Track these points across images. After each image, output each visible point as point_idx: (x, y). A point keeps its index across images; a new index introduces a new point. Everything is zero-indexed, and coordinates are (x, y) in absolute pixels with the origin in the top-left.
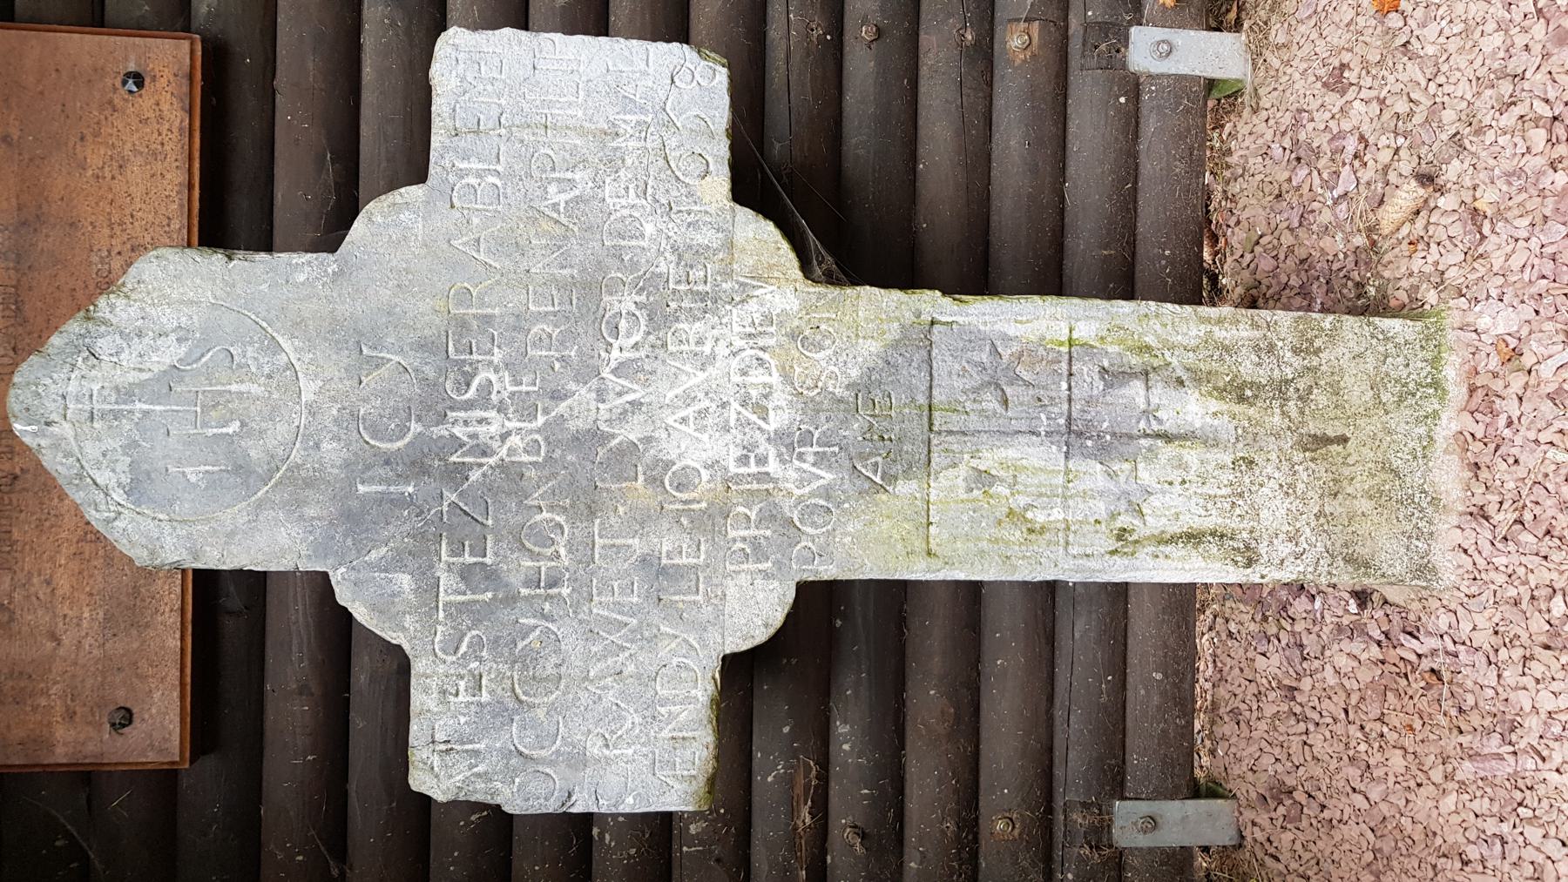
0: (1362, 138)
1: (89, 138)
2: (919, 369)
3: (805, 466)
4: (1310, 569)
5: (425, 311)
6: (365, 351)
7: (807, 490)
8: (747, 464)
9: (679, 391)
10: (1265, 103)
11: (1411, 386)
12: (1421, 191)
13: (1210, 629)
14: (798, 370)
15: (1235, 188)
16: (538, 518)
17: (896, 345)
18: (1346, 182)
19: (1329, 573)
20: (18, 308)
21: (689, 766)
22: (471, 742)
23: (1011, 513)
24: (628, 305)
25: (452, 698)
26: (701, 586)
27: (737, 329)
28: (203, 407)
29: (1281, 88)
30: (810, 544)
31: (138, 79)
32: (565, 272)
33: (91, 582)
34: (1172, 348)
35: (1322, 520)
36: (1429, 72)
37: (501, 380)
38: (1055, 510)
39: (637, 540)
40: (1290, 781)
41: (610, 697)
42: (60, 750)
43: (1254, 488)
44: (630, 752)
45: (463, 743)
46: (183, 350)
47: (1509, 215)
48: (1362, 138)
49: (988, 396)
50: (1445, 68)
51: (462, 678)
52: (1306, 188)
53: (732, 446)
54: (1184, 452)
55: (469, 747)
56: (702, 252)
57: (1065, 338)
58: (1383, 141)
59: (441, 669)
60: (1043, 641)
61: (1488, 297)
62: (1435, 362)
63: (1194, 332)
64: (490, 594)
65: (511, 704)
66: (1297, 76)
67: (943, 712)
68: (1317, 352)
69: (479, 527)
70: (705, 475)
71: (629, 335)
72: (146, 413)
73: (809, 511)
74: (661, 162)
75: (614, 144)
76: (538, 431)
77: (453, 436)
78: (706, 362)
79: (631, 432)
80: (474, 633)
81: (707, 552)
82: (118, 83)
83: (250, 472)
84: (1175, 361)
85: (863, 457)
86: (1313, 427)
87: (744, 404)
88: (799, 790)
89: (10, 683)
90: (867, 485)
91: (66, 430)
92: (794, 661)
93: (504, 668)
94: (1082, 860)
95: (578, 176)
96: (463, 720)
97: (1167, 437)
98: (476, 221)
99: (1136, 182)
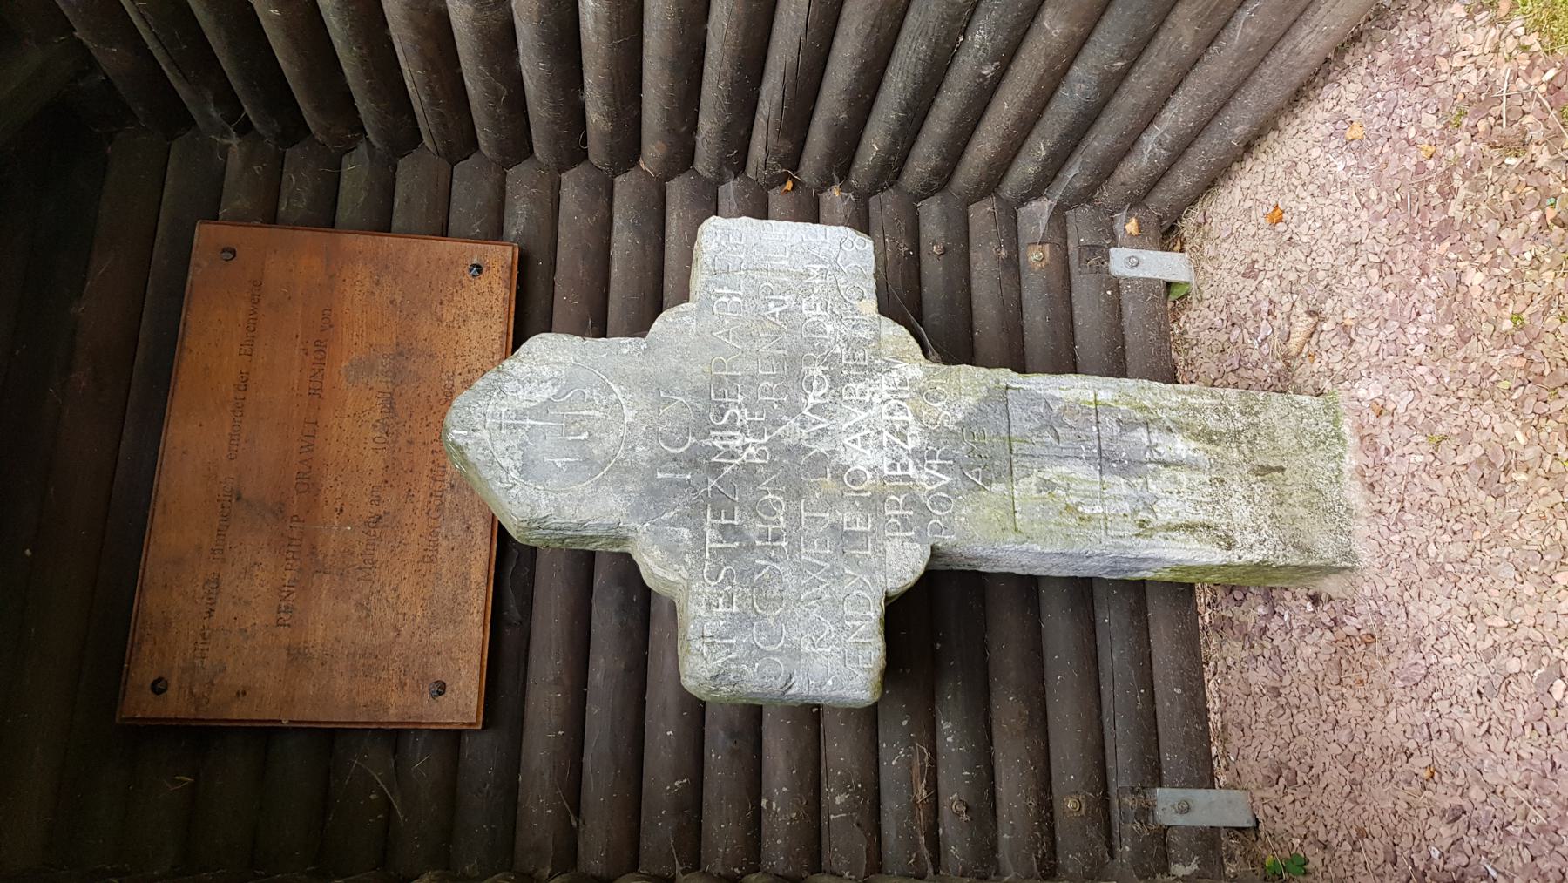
0: (1271, 302)
1: (445, 303)
2: (1001, 414)
3: (932, 472)
4: (1271, 552)
5: (697, 371)
6: (662, 395)
7: (934, 487)
8: (895, 469)
9: (851, 423)
10: (1206, 295)
11: (1322, 436)
12: (1310, 320)
13: (1214, 674)
14: (924, 413)
15: (1193, 354)
16: (766, 497)
17: (985, 399)
18: (1265, 329)
19: (1285, 556)
20: (392, 407)
21: (868, 661)
22: (727, 638)
23: (1067, 507)
24: (818, 372)
25: (714, 609)
26: (870, 545)
27: (885, 387)
28: (566, 423)
29: (1215, 284)
30: (938, 521)
31: (479, 268)
32: (781, 352)
33: (425, 590)
34: (1161, 408)
35: (1274, 520)
36: (1306, 252)
37: (742, 413)
38: (1097, 507)
39: (828, 515)
40: (1284, 757)
41: (814, 614)
42: (392, 711)
43: (1226, 498)
44: (829, 650)
45: (722, 639)
46: (556, 390)
47: (1364, 323)
48: (1271, 302)
49: (1046, 434)
50: (1315, 248)
51: (721, 596)
52: (1240, 341)
53: (885, 458)
54: (1177, 473)
55: (725, 641)
56: (862, 343)
57: (1092, 400)
58: (1285, 299)
59: (708, 590)
60: (1090, 662)
61: (1362, 376)
62: (1335, 422)
63: (1174, 399)
64: (737, 544)
65: (752, 615)
66: (1225, 274)
67: (1020, 714)
68: (1256, 414)
69: (730, 501)
70: (869, 475)
71: (819, 389)
72: (532, 426)
73: (937, 501)
74: (835, 291)
75: (807, 281)
76: (765, 445)
77: (713, 446)
78: (867, 407)
79: (822, 447)
80: (728, 567)
81: (872, 523)
82: (466, 270)
83: (593, 463)
84: (1164, 416)
85: (970, 468)
86: (1260, 461)
87: (892, 432)
88: (916, 770)
89: (362, 661)
90: (973, 485)
91: (485, 434)
92: (908, 671)
93: (747, 591)
94: (1136, 835)
95: (786, 298)
96: (722, 623)
97: (1166, 465)
98: (727, 322)
99: (1123, 346)
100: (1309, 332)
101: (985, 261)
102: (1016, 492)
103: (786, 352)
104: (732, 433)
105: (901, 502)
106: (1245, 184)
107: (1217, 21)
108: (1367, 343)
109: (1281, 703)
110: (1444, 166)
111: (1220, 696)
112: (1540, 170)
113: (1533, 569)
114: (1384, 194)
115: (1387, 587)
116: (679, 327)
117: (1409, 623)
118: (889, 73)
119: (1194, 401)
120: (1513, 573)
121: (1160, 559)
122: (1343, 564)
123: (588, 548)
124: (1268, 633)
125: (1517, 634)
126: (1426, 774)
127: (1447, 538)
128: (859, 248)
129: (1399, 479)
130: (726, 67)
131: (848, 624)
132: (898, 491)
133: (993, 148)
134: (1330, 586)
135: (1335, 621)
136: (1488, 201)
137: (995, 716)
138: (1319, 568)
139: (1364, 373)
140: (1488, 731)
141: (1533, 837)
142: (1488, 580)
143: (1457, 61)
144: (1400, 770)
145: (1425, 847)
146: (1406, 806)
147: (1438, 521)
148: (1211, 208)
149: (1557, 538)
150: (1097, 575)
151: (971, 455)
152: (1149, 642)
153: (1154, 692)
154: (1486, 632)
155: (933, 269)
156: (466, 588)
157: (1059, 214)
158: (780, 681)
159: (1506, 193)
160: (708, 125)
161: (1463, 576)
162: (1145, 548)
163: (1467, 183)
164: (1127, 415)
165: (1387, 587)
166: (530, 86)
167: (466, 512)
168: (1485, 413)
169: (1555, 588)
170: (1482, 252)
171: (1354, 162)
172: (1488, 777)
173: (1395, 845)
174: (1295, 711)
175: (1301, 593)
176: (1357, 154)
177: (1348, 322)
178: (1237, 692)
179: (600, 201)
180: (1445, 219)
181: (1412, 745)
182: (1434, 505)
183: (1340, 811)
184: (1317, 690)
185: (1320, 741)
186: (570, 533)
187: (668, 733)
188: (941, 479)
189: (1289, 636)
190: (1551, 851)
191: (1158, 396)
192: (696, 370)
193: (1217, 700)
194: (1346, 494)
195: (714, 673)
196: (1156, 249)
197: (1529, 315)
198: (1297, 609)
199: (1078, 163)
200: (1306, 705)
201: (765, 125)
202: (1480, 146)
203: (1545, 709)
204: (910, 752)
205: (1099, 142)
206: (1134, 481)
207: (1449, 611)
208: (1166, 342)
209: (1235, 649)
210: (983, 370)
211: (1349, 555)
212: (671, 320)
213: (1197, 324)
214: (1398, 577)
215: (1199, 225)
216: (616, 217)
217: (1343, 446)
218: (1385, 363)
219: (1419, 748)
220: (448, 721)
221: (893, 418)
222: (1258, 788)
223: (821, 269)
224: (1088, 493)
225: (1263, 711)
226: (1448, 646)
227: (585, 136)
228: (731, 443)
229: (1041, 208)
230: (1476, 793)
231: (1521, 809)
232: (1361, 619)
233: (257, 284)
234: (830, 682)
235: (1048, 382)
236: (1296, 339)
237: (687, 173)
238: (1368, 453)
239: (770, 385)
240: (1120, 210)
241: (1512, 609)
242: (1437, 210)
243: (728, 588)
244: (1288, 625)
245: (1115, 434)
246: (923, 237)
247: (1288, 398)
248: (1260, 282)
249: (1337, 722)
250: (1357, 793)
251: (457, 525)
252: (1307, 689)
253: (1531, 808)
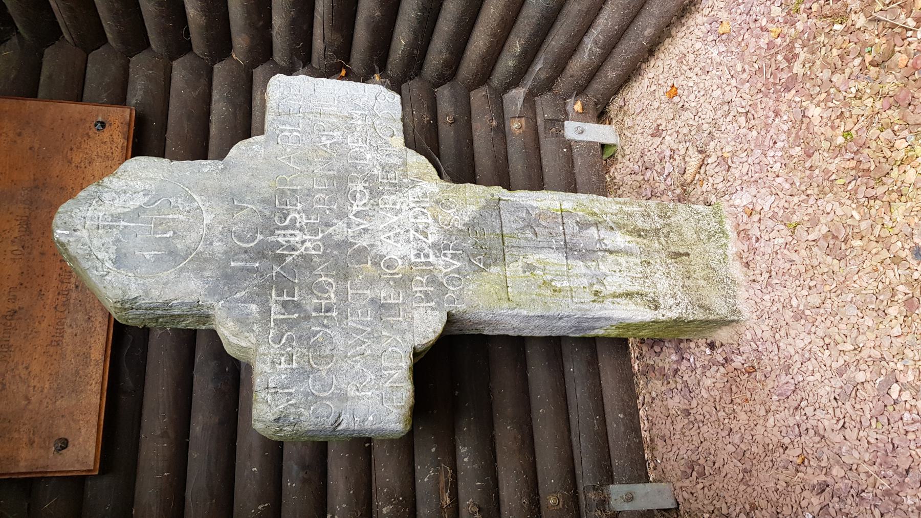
0: (671, 150)
2: (495, 218)
3: (447, 259)
4: (684, 311)
5: (265, 186)
6: (236, 203)
7: (449, 270)
10: (627, 152)
11: (712, 232)
12: (700, 156)
13: (643, 405)
14: (440, 217)
16: (320, 280)
17: (484, 207)
18: (668, 168)
20: (28, 227)
21: (400, 401)
22: (288, 388)
23: (544, 283)
25: (277, 366)
26: (401, 313)
27: (411, 199)
28: (155, 224)
29: (633, 144)
30: (452, 295)
31: (103, 125)
32: (331, 173)
33: (52, 367)
34: (606, 213)
35: (685, 289)
36: (694, 112)
37: (301, 217)
39: (369, 291)
40: (695, 458)
41: (358, 366)
42: (22, 464)
43: (652, 274)
44: (370, 393)
45: (283, 389)
46: (146, 199)
48: (671, 150)
51: (283, 355)
53: (412, 250)
54: (618, 258)
55: (287, 391)
56: (393, 167)
57: (558, 208)
59: (272, 351)
62: (720, 222)
63: (614, 208)
64: (297, 315)
67: (515, 438)
68: (669, 217)
69: (291, 283)
70: (400, 262)
71: (361, 200)
72: (125, 227)
75: (351, 122)
76: (319, 240)
77: (278, 241)
79: (364, 242)
80: (289, 333)
81: (403, 297)
83: (177, 255)
84: (608, 219)
85: (474, 256)
86: (673, 249)
87: (416, 231)
88: (442, 484)
90: (477, 268)
91: (84, 234)
96: (283, 377)
98: (289, 150)
100: (699, 165)
101: (482, 128)
102: (508, 273)
103: (335, 173)
104: (293, 232)
105: (424, 281)
106: (651, 75)
108: (740, 167)
109: (691, 420)
110: (788, 41)
111: (648, 419)
112: (859, 29)
113: (871, 307)
114: (746, 67)
115: (763, 331)
116: (251, 154)
117: (780, 355)
119: (627, 209)
120: (855, 311)
121: (610, 318)
122: (732, 318)
123: (179, 327)
124: (679, 373)
125: (862, 354)
126: (799, 461)
127: (805, 292)
128: (390, 100)
129: (767, 257)
131: (385, 373)
133: (485, 44)
134: (722, 335)
135: (726, 359)
136: (821, 59)
137: (498, 441)
138: (715, 321)
139: (738, 188)
140: (843, 426)
141: (881, 499)
142: (838, 318)
144: (779, 459)
145: (801, 513)
146: (785, 485)
147: (797, 282)
148: (628, 96)
149: (888, 283)
150: (565, 334)
151: (475, 246)
152: (600, 384)
153: (605, 418)
154: (838, 355)
155: (447, 133)
156: (87, 365)
157: (530, 97)
158: (331, 420)
159: (834, 50)
161: (818, 317)
162: (598, 310)
163: (805, 49)
164: (583, 219)
165: (763, 331)
167: (88, 306)
168: (828, 202)
169: (888, 318)
170: (819, 93)
171: (724, 49)
172: (847, 459)
173: (778, 513)
174: (701, 425)
175: (702, 342)
176: (727, 44)
177: (726, 155)
178: (660, 415)
179: (202, 80)
180: (790, 76)
181: (787, 441)
182: (794, 271)
183: (736, 492)
184: (716, 409)
185: (720, 444)
186: (159, 312)
187: (253, 469)
188: (454, 264)
189: (694, 373)
190: (896, 509)
191: (603, 205)
192: (263, 184)
193: (646, 422)
194: (731, 270)
195: (277, 416)
196: (594, 122)
197: (856, 131)
198: (699, 353)
199: (542, 59)
200: (708, 419)
201: (321, 21)
202: (814, 21)
203: (886, 406)
204: (438, 471)
205: (556, 41)
206: (589, 264)
207: (810, 343)
208: (603, 183)
209: (657, 386)
210: (482, 187)
211: (735, 311)
212: (244, 148)
213: (622, 172)
214: (770, 324)
215: (621, 107)
216: (215, 92)
217: (726, 238)
218: (753, 179)
219: (792, 442)
220: (70, 469)
221: (418, 221)
222: (678, 480)
223: (362, 114)
224: (558, 273)
225: (678, 427)
226: (811, 368)
227: (187, 30)
228: (292, 239)
229: (518, 94)
230: (837, 471)
231: (871, 480)
232: (745, 356)
234: (371, 418)
235: (528, 195)
236: (690, 171)
237: (268, 63)
238: (744, 242)
239: (324, 197)
240: (570, 97)
241: (857, 337)
242: (785, 71)
243: (289, 349)
244: (693, 365)
245: (575, 231)
246: (439, 112)
247: (689, 207)
248: (664, 138)
249: (731, 429)
250: (748, 479)
251: (80, 316)
252: (709, 409)
253: (879, 478)
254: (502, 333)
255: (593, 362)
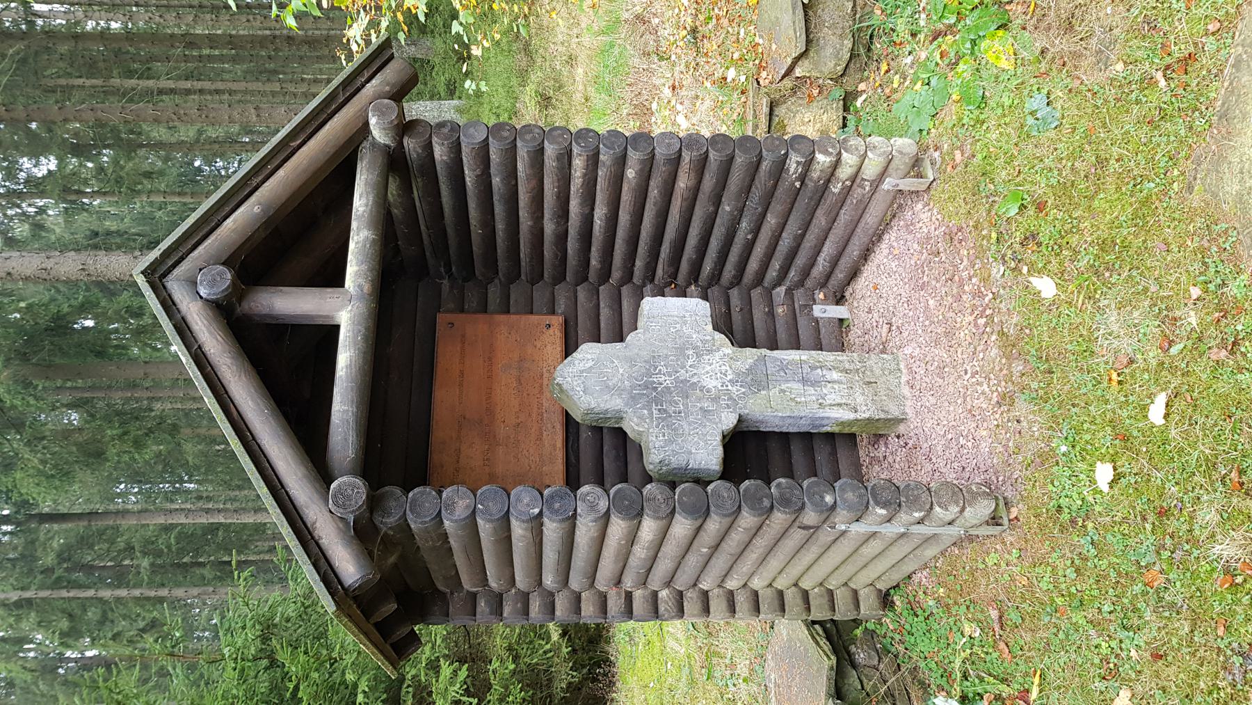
5: (645, 354)
24: (691, 352)
62: (898, 364)
79: (695, 380)
86: (867, 380)
106: (865, 275)
107: (833, 214)
118: (711, 239)
130: (648, 241)
132: (725, 395)
134: (902, 429)
143: (921, 225)
155: (736, 317)
156: (555, 450)
157: (789, 292)
158: (685, 463)
160: (639, 263)
162: (821, 413)
166: (570, 251)
205: (800, 261)
211: (904, 413)
229: (781, 290)
233: (463, 336)
254: (771, 429)
255: (834, 453)
